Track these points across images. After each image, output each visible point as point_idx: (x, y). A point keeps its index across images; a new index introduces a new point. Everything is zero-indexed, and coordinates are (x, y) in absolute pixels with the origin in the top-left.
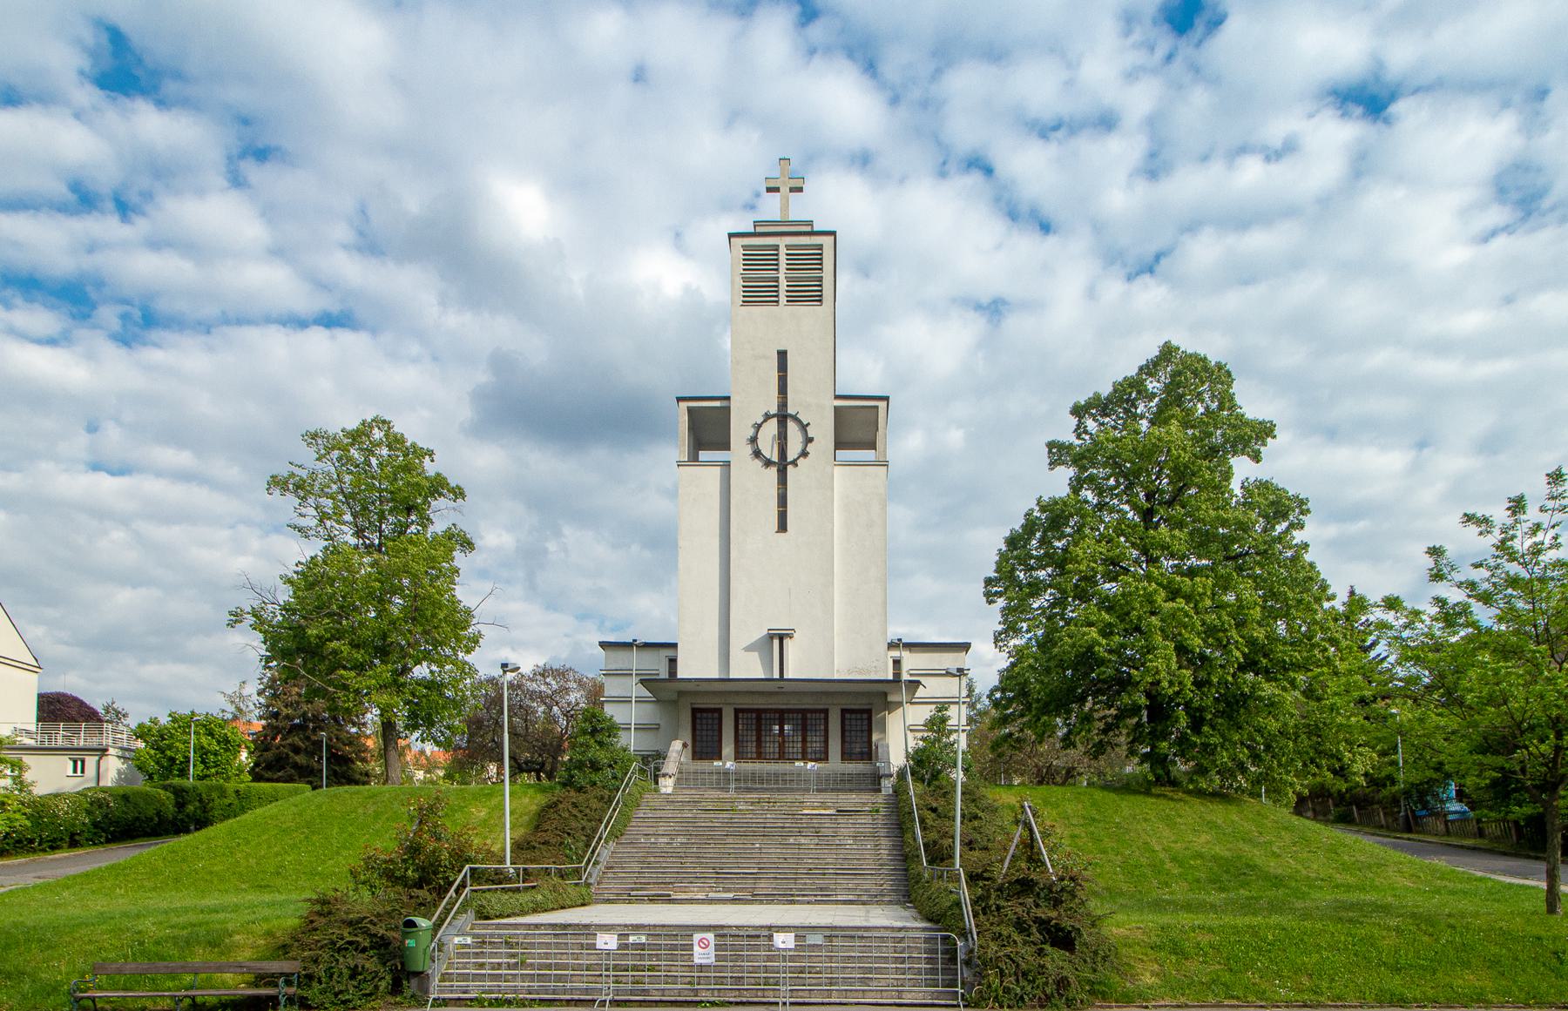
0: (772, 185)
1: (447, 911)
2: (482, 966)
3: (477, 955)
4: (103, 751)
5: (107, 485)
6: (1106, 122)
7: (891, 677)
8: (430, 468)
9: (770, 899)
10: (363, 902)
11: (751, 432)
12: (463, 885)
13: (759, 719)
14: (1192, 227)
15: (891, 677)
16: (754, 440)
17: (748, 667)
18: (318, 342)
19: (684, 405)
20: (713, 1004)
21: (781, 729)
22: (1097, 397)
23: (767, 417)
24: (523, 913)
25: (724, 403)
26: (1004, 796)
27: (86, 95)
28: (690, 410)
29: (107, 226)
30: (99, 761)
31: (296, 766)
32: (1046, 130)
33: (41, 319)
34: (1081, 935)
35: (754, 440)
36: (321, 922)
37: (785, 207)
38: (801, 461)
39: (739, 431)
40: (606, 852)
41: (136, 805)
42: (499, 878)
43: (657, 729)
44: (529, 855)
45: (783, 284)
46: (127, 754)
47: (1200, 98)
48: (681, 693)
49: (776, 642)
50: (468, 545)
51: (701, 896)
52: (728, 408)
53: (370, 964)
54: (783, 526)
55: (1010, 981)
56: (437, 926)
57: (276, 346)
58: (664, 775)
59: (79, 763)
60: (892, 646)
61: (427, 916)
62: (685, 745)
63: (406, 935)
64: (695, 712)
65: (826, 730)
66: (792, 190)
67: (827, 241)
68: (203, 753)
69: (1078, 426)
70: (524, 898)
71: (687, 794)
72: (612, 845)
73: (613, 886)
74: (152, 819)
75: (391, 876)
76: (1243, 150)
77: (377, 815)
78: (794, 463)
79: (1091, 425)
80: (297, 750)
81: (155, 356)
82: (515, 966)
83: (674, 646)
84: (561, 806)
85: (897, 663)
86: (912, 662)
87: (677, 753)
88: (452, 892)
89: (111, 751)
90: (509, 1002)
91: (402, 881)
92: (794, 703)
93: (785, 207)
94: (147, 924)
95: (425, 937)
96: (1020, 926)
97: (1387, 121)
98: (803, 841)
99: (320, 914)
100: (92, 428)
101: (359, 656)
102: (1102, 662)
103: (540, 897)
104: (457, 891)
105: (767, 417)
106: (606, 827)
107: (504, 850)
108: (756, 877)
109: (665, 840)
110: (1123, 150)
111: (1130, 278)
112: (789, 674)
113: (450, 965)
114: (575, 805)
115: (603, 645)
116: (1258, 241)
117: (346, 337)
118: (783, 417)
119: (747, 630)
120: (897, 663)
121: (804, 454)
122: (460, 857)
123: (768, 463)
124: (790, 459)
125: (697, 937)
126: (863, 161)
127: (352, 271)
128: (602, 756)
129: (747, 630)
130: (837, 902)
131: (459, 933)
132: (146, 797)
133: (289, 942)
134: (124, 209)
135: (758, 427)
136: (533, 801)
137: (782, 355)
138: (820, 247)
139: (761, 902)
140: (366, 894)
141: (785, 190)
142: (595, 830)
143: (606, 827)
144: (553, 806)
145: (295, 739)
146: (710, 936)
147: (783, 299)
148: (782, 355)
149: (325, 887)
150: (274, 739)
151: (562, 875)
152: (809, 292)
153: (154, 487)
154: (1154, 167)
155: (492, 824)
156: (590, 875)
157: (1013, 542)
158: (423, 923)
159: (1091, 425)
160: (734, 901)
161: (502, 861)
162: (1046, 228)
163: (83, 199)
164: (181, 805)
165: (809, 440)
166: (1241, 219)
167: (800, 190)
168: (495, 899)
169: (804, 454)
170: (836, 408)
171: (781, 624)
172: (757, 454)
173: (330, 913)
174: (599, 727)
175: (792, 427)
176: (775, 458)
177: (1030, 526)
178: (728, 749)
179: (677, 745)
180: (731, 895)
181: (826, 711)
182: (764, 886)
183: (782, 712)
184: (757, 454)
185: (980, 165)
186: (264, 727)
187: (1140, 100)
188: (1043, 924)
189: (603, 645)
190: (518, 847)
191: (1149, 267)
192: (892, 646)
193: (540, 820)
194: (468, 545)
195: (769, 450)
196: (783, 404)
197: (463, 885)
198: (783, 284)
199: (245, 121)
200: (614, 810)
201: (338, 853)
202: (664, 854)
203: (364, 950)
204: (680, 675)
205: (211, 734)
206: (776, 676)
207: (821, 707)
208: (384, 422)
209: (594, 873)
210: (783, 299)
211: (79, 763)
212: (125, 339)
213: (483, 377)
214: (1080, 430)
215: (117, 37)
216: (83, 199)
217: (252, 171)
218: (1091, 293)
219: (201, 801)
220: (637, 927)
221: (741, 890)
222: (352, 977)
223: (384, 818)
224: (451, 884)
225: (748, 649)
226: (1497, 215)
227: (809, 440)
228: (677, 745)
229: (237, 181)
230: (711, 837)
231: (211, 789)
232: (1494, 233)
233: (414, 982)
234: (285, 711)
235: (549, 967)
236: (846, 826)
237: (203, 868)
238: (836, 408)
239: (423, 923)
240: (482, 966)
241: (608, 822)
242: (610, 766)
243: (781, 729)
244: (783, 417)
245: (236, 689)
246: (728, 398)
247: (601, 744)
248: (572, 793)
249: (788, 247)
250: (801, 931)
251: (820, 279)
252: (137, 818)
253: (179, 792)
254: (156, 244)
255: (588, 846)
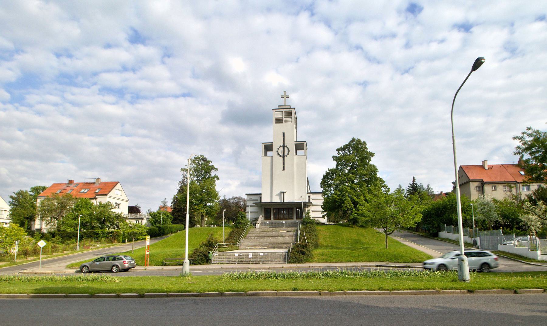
0: (282, 97)
1: (214, 251)
2: (219, 259)
3: (218, 257)
4: (142, 219)
5: (125, 139)
6: (394, 36)
7: (308, 201)
8: (210, 164)
9: (271, 248)
10: (202, 249)
11: (277, 150)
12: (217, 247)
13: (279, 210)
14: (418, 61)
15: (308, 201)
16: (278, 151)
17: (276, 200)
18: (182, 102)
19: (263, 144)
20: (252, 263)
21: (283, 212)
22: (341, 147)
23: (280, 146)
24: (226, 251)
25: (271, 144)
26: (318, 228)
27: (127, 44)
28: (264, 145)
29: (129, 75)
30: (141, 221)
31: (179, 220)
32: (375, 38)
33: (111, 98)
34: (305, 253)
35: (278, 151)
36: (196, 252)
37: (285, 101)
38: (287, 156)
39: (275, 148)
40: (242, 240)
41: (152, 231)
42: (222, 245)
43: (258, 212)
44: (228, 241)
45: (284, 119)
46: (148, 219)
47: (418, 28)
48: (262, 205)
49: (282, 194)
50: (218, 178)
51: (259, 248)
52: (272, 145)
53: (203, 258)
54: (284, 169)
55: (294, 259)
56: (213, 253)
57: (171, 103)
58: (257, 223)
59: (138, 221)
60: (308, 193)
61: (211, 251)
62: (263, 216)
63: (208, 254)
64: (265, 209)
65: (293, 212)
66: (286, 98)
67: (293, 110)
68: (163, 218)
69: (338, 153)
70: (226, 249)
71: (263, 228)
72: (243, 239)
73: (243, 247)
74: (154, 234)
75: (205, 245)
76: (431, 41)
77: (201, 233)
78: (286, 156)
79: (341, 152)
80: (179, 216)
81: (139, 106)
82: (224, 259)
83: (261, 194)
84: (234, 232)
85: (309, 197)
86: (312, 196)
87: (261, 218)
88: (215, 248)
89: (144, 219)
90: (223, 264)
91: (207, 246)
92: (286, 207)
93: (285, 101)
94: (169, 253)
95: (211, 254)
96: (297, 252)
97: (471, 32)
98: (279, 237)
99: (196, 251)
100: (123, 125)
101: (197, 202)
102: (337, 202)
103: (229, 248)
104: (216, 248)
105: (280, 146)
106: (243, 235)
107: (223, 240)
108: (269, 244)
109: (254, 238)
110: (399, 42)
111: (402, 74)
112: (285, 201)
113: (215, 258)
114: (237, 231)
115: (246, 194)
116: (437, 64)
117: (189, 99)
118: (284, 146)
119: (276, 191)
120: (309, 197)
121: (288, 154)
122: (216, 242)
123: (281, 156)
124: (285, 155)
125: (249, 254)
126: (328, 48)
127: (191, 83)
128: (242, 222)
129: (276, 191)
130: (282, 249)
131: (216, 254)
132: (154, 229)
133: (192, 255)
134: (134, 70)
135: (279, 149)
136: (229, 230)
137: (284, 134)
138: (291, 111)
139: (269, 249)
140: (202, 248)
141: (285, 98)
142: (240, 236)
143: (243, 235)
144: (233, 232)
145: (179, 214)
146: (251, 254)
147: (284, 122)
148: (284, 134)
149: (197, 248)
150: (174, 213)
151: (234, 245)
152: (289, 119)
153: (137, 140)
154: (408, 46)
155: (221, 235)
156: (239, 244)
157: (324, 176)
158: (211, 252)
159: (341, 152)
160: (264, 249)
161: (223, 243)
162: (379, 63)
163: (125, 69)
164: (159, 230)
165: (289, 151)
166: (433, 58)
167: (288, 97)
168: (222, 249)
169: (288, 154)
170: (295, 144)
171: (283, 190)
172: (278, 154)
173: (197, 251)
174: (242, 216)
175: (286, 148)
176: (282, 155)
177: (327, 174)
178: (272, 217)
179: (261, 216)
180: (264, 248)
181: (293, 208)
182: (270, 246)
183: (283, 208)
184: (278, 154)
185: (358, 47)
186: (172, 211)
187: (402, 30)
188: (300, 251)
189: (246, 194)
190: (226, 240)
191: (407, 71)
192: (308, 193)
193: (231, 234)
194: (218, 178)
195: (281, 154)
196: (284, 144)
197: (217, 247)
198: (284, 119)
199: (166, 48)
200: (244, 232)
201: (194, 241)
202: (253, 240)
203: (202, 256)
204: (262, 202)
205: (165, 215)
206: (282, 201)
207: (292, 207)
208: (202, 156)
209: (240, 244)
210: (284, 122)
211: (138, 221)
212: (132, 103)
213: (225, 108)
214: (339, 154)
215: (135, 31)
216: (125, 69)
217: (167, 60)
218: (392, 79)
219: (163, 229)
220: (241, 253)
221: (266, 247)
222: (201, 260)
223: (202, 234)
224: (215, 247)
225: (277, 195)
226: (505, 54)
227: (289, 151)
228: (261, 216)
229: (163, 63)
230: (262, 237)
231: (165, 227)
232: (505, 59)
233: (210, 261)
234: (177, 207)
235: (228, 259)
236: (288, 234)
237: (171, 244)
238: (295, 144)
239: (211, 252)
240: (219, 259)
241: (243, 234)
242: (244, 224)
243: (283, 212)
244: (284, 146)
245: (164, 200)
246: (272, 143)
247: (243, 219)
248: (237, 229)
249: (285, 111)
250: (264, 253)
251: (291, 118)
252: (152, 234)
253: (159, 228)
254: (142, 78)
255: (239, 239)
